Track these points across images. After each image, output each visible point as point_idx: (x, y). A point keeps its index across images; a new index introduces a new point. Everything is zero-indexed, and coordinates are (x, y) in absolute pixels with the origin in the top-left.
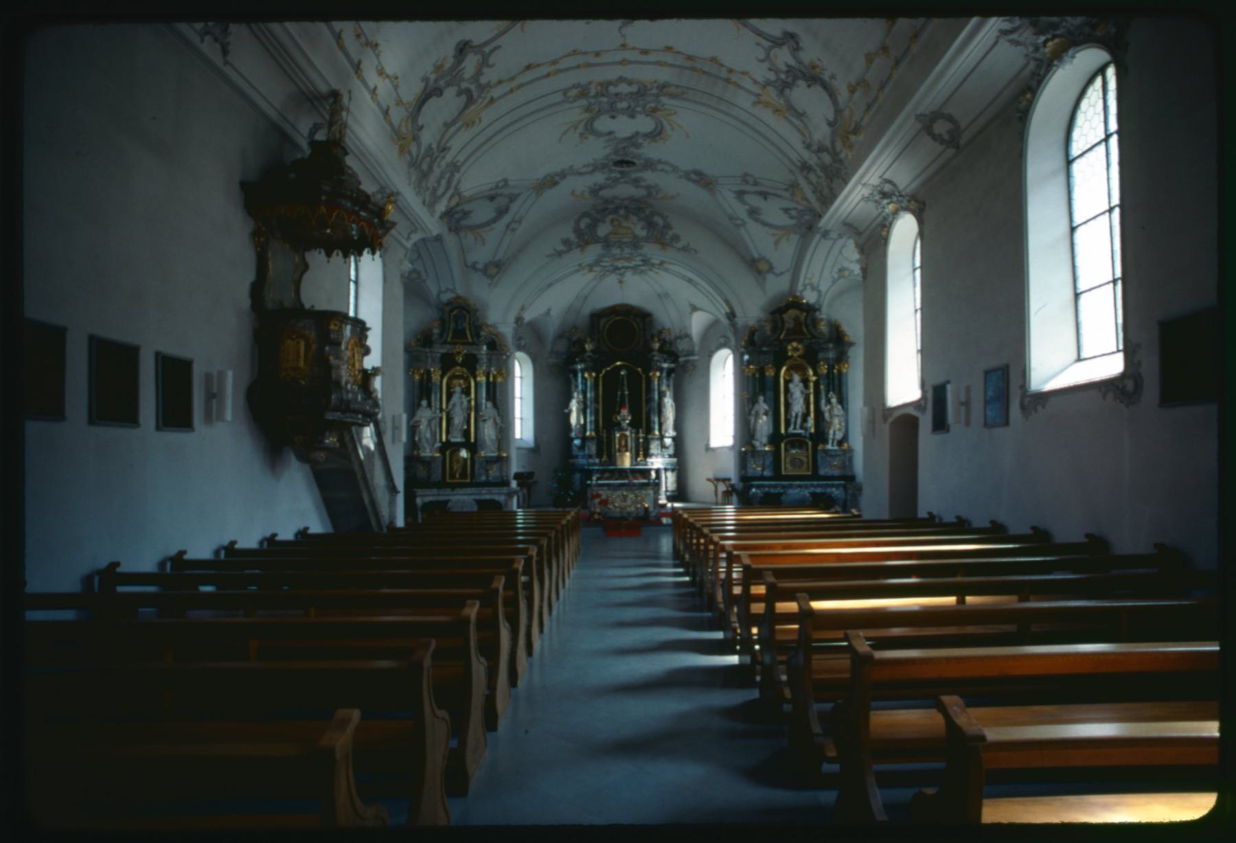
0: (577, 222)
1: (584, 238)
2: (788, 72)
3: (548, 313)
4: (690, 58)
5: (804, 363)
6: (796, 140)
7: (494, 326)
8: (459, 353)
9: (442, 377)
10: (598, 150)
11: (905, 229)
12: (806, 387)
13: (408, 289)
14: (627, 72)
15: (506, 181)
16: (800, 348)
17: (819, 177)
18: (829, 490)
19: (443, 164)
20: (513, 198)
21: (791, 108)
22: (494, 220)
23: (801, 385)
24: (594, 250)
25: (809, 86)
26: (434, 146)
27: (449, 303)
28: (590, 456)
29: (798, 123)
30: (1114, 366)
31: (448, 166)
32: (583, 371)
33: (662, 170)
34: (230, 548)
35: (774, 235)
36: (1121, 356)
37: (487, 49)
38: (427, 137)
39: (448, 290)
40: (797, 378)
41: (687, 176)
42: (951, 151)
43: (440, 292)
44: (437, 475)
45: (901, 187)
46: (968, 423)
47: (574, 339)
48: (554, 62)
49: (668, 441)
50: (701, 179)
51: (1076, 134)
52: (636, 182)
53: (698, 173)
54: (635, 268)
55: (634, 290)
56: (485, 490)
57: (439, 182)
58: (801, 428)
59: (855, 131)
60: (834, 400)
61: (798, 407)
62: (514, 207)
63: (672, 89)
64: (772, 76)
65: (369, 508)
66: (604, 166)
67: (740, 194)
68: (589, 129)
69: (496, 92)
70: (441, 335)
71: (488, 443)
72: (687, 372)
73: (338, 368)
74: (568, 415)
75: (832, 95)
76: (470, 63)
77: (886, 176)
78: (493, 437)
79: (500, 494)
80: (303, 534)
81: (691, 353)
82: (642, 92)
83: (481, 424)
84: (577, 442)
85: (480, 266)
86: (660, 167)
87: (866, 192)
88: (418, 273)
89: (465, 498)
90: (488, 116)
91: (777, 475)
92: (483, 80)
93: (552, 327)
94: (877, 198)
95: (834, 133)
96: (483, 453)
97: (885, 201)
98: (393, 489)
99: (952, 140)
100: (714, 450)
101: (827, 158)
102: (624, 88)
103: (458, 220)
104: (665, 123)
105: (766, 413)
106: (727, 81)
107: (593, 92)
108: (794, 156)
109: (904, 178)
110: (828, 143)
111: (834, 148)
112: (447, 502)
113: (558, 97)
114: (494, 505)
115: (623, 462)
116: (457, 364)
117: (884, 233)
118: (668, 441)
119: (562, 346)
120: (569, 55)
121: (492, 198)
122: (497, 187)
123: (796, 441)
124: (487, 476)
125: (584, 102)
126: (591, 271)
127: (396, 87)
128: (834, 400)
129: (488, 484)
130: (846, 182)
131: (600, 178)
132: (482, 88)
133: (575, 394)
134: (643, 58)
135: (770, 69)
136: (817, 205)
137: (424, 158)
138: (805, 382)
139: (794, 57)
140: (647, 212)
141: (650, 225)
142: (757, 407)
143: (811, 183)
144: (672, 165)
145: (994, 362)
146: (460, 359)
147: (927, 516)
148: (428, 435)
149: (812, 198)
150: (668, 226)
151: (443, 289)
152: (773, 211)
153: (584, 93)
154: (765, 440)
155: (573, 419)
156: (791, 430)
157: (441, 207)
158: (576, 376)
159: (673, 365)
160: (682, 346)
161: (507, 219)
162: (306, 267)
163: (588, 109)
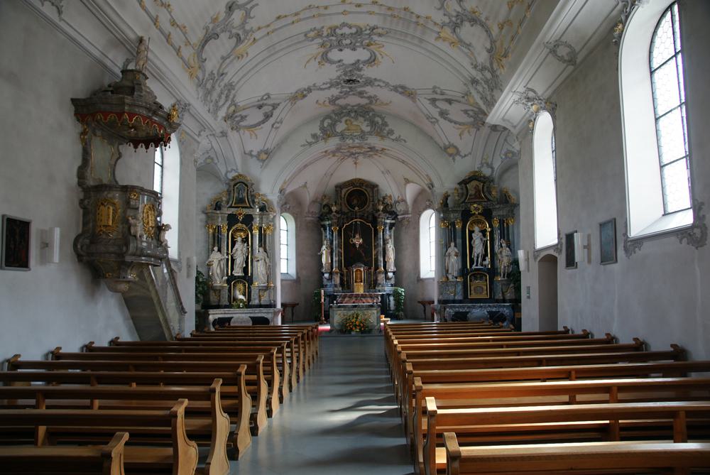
0: (323, 122)
1: (327, 133)
2: (457, 16)
3: (305, 186)
4: (389, 8)
5: (483, 218)
6: (466, 63)
7: (264, 195)
8: (240, 214)
9: (228, 231)
10: (332, 73)
11: (544, 123)
12: (484, 235)
13: (198, 170)
14: (349, 19)
15: (269, 96)
16: (483, 206)
17: (484, 88)
18: (501, 310)
19: (222, 84)
20: (275, 106)
21: (461, 41)
22: (263, 122)
23: (481, 234)
24: (333, 143)
25: (472, 26)
26: (215, 72)
27: (234, 179)
28: (336, 286)
29: (466, 51)
30: (687, 219)
31: (226, 85)
32: (330, 226)
33: (379, 85)
34: (56, 354)
35: (458, 129)
36: (691, 211)
37: (249, 6)
38: (211, 65)
39: (232, 170)
40: (476, 229)
41: (395, 89)
42: (571, 68)
43: (227, 172)
44: (225, 301)
45: (540, 93)
46: (589, 261)
47: (324, 203)
48: (296, 14)
49: (390, 275)
50: (403, 90)
51: (655, 53)
52: (361, 94)
53: (403, 87)
54: (364, 153)
55: (367, 171)
56: (257, 310)
57: (220, 97)
58: (482, 265)
59: (505, 56)
60: (504, 245)
61: (478, 249)
62: (276, 113)
63: (380, 31)
64: (446, 20)
65: (164, 325)
66: (338, 84)
67: (433, 101)
68: (325, 58)
69: (258, 35)
70: (228, 202)
71: (261, 277)
72: (406, 228)
73: (135, 225)
74: (321, 256)
75: (488, 31)
76: (237, 16)
77: (529, 86)
78: (264, 272)
79: (268, 313)
80: (114, 342)
81: (406, 212)
82: (359, 32)
83: (255, 263)
84: (326, 275)
85: (254, 153)
86: (376, 83)
87: (516, 97)
88: (212, 159)
89: (243, 315)
90: (253, 51)
91: (466, 299)
92: (247, 27)
93: (308, 196)
94: (524, 101)
95: (491, 57)
96: (256, 284)
97: (530, 104)
98: (182, 311)
99: (571, 61)
100: (423, 280)
101: (489, 75)
102: (346, 31)
103: (238, 122)
104: (377, 53)
105: (456, 255)
106: (417, 23)
107: (325, 34)
108: (466, 74)
109: (541, 88)
110: (488, 65)
111: (492, 68)
112: (232, 318)
113: (302, 37)
114: (265, 321)
115: (358, 290)
116: (237, 221)
117: (531, 126)
118: (390, 275)
119: (315, 209)
120: (306, 9)
121: (260, 107)
122: (262, 99)
123: (478, 274)
124: (260, 301)
125: (319, 40)
126: (334, 156)
127: (185, 34)
128: (504, 245)
129: (260, 306)
130: (502, 91)
131: (335, 92)
132: (246, 32)
133: (325, 242)
134: (358, 9)
135: (445, 15)
136: (484, 107)
137: (208, 80)
138: (484, 232)
139: (460, 6)
140: (371, 114)
141: (372, 123)
142: (450, 250)
143: (478, 92)
144: (384, 82)
145: (603, 217)
146: (241, 218)
147: (563, 330)
148: (219, 271)
149: (481, 103)
150: (385, 124)
151: (229, 169)
152: (455, 112)
153: (319, 35)
154: (455, 274)
155: (324, 260)
156: (474, 267)
157: (222, 113)
158: (325, 229)
159: (393, 221)
160: (400, 208)
161: (272, 120)
162: (120, 155)
163: (323, 45)
